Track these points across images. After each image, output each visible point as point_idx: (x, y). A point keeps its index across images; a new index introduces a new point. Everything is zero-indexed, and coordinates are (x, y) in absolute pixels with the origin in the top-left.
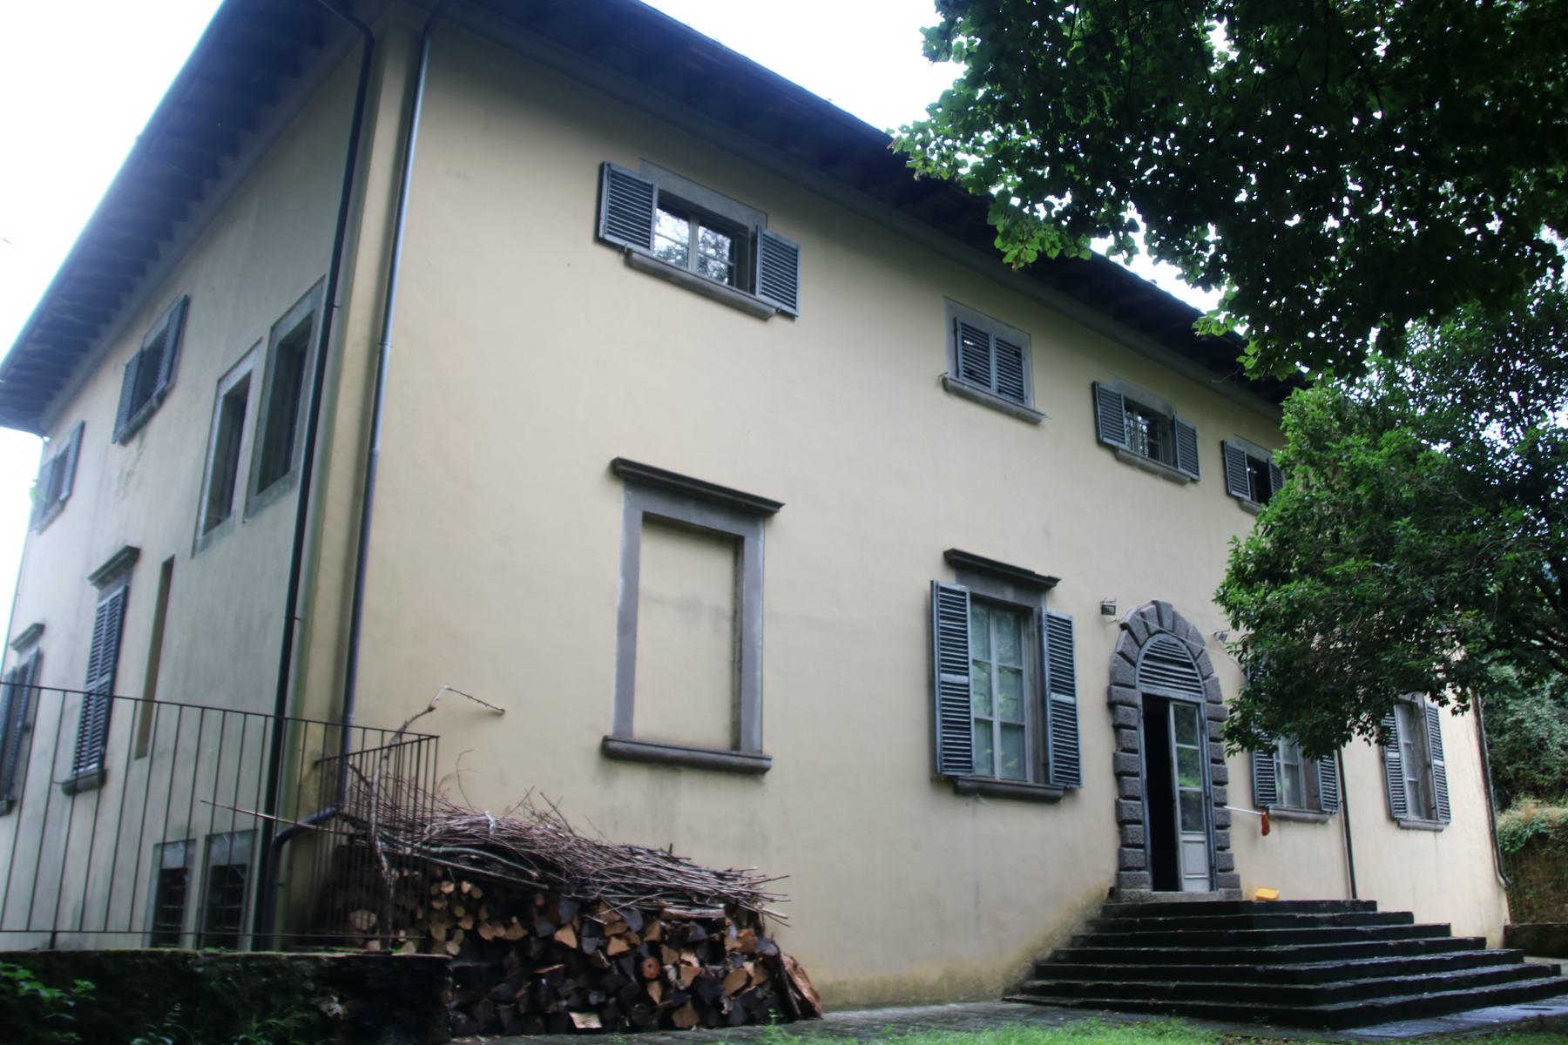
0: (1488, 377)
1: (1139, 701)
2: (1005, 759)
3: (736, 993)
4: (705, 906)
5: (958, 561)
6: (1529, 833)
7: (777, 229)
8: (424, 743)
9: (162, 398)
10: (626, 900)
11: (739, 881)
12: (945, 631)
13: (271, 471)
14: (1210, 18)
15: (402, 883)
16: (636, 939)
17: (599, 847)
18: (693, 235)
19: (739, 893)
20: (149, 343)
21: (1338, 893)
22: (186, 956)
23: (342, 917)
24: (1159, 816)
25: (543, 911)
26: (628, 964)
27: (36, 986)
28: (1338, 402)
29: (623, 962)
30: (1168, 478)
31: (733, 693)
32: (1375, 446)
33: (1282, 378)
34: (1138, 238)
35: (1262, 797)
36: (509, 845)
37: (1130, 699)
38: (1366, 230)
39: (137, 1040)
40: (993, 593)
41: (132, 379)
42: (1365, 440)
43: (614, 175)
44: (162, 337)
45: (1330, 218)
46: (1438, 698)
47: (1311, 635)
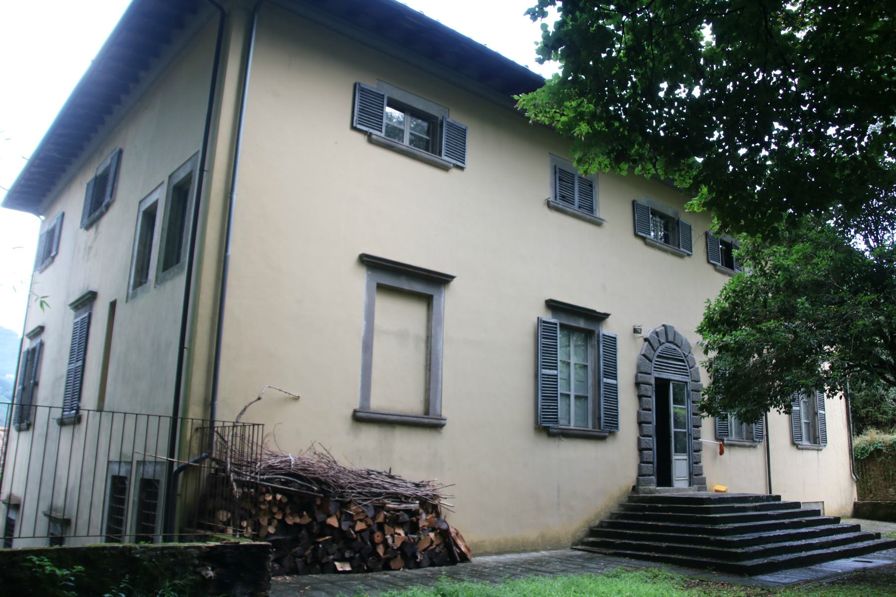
1: (653, 382)
3: (425, 550)
4: (409, 503)
5: (553, 305)
6: (872, 449)
7: (455, 118)
8: (256, 427)
9: (108, 207)
10: (366, 500)
11: (428, 488)
12: (545, 346)
13: (170, 260)
15: (244, 496)
16: (370, 522)
19: (427, 495)
20: (100, 172)
22: (130, 549)
23: (213, 514)
24: (663, 443)
25: (320, 507)
26: (366, 535)
27: (54, 568)
29: (364, 534)
30: (674, 254)
35: (720, 435)
36: (301, 473)
37: (648, 381)
38: (783, 155)
39: (107, 595)
40: (573, 323)
43: (362, 90)
45: (764, 150)
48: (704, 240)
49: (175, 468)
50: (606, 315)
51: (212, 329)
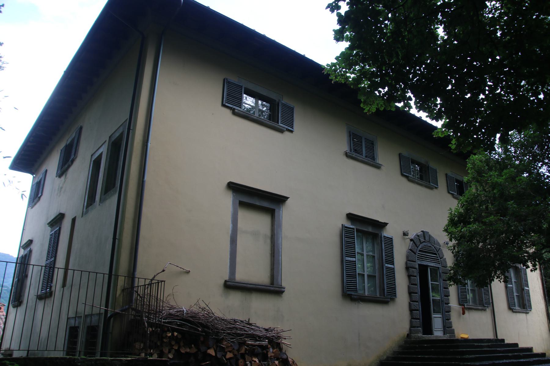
0: (541, 150)
1: (417, 267)
2: (369, 288)
5: (351, 217)
7: (286, 101)
8: (160, 283)
9: (72, 162)
10: (233, 338)
12: (347, 242)
13: (108, 188)
14: (437, 25)
16: (236, 353)
17: (223, 320)
18: (257, 103)
19: (273, 336)
20: (69, 142)
21: (491, 336)
24: (425, 307)
28: (487, 159)
31: (271, 265)
32: (500, 175)
33: (465, 152)
34: (412, 103)
35: (462, 301)
36: (191, 319)
38: (493, 98)
40: (363, 230)
41: (63, 155)
42: (497, 173)
43: (229, 83)
44: (73, 140)
45: (481, 95)
46: (525, 266)
47: (478, 244)
48: (445, 179)
49: (109, 315)
50: (386, 224)
51: (134, 227)
